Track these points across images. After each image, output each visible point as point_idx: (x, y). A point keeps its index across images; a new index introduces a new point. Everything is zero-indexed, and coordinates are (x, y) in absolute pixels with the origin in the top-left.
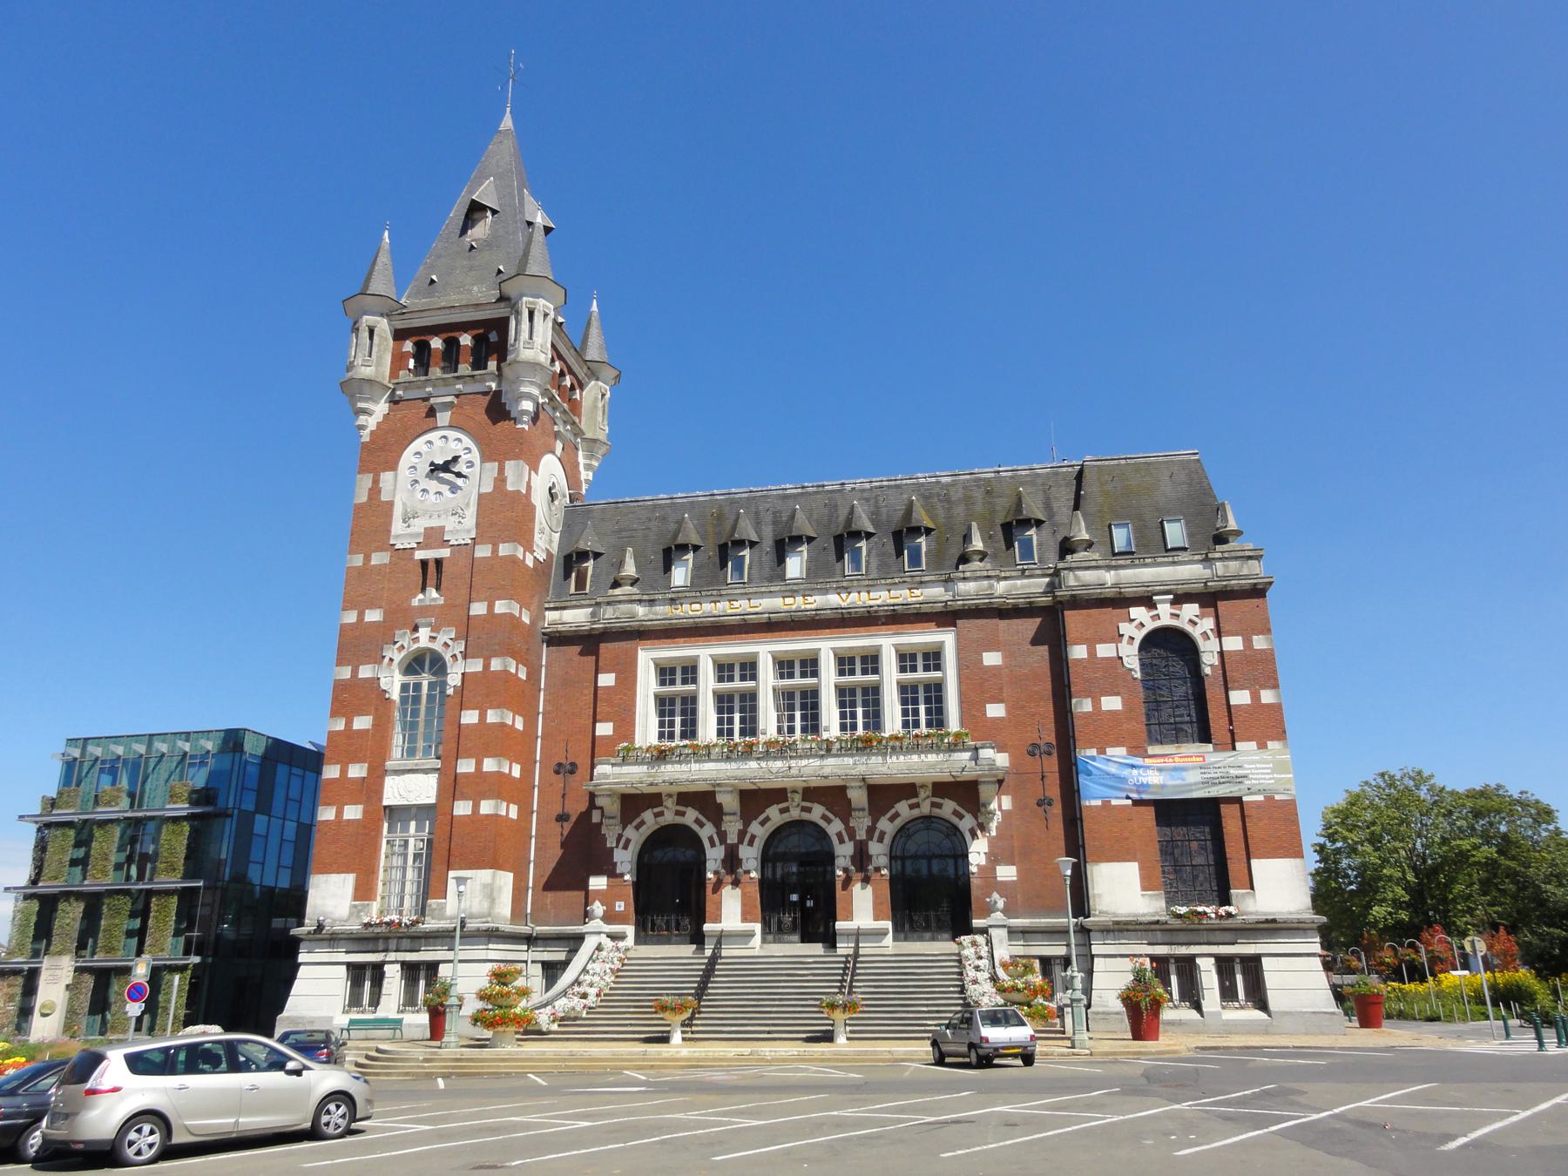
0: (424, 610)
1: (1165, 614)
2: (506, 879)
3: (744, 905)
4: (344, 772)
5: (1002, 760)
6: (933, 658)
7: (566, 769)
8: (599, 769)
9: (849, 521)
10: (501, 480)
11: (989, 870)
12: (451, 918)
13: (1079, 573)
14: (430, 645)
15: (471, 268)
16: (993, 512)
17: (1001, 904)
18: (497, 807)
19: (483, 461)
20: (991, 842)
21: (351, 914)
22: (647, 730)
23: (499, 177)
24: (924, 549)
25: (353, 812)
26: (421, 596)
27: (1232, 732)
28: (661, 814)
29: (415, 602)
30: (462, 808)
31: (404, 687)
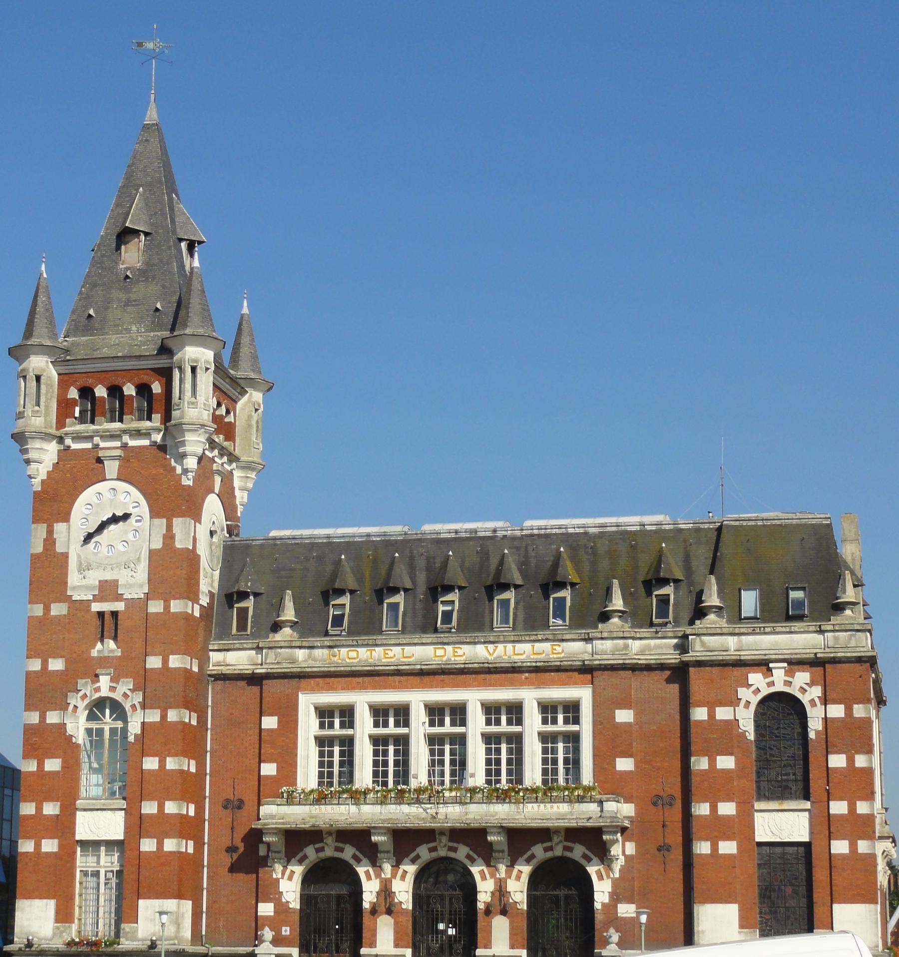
0: (104, 661)
1: (779, 681)
2: (187, 905)
3: (396, 932)
4: (39, 809)
5: (627, 810)
6: (572, 710)
7: (234, 805)
8: (265, 810)
9: (498, 572)
10: (169, 537)
11: (610, 908)
12: (142, 940)
13: (705, 639)
14: (111, 695)
15: (128, 303)
16: (636, 567)
17: (615, 937)
18: (179, 845)
19: (151, 518)
20: (615, 883)
21: (54, 935)
22: (308, 775)
23: (149, 186)
24: (568, 603)
25: (50, 846)
26: (99, 646)
27: (828, 791)
28: (322, 849)
29: (94, 653)
30: (148, 845)
31: (89, 731)
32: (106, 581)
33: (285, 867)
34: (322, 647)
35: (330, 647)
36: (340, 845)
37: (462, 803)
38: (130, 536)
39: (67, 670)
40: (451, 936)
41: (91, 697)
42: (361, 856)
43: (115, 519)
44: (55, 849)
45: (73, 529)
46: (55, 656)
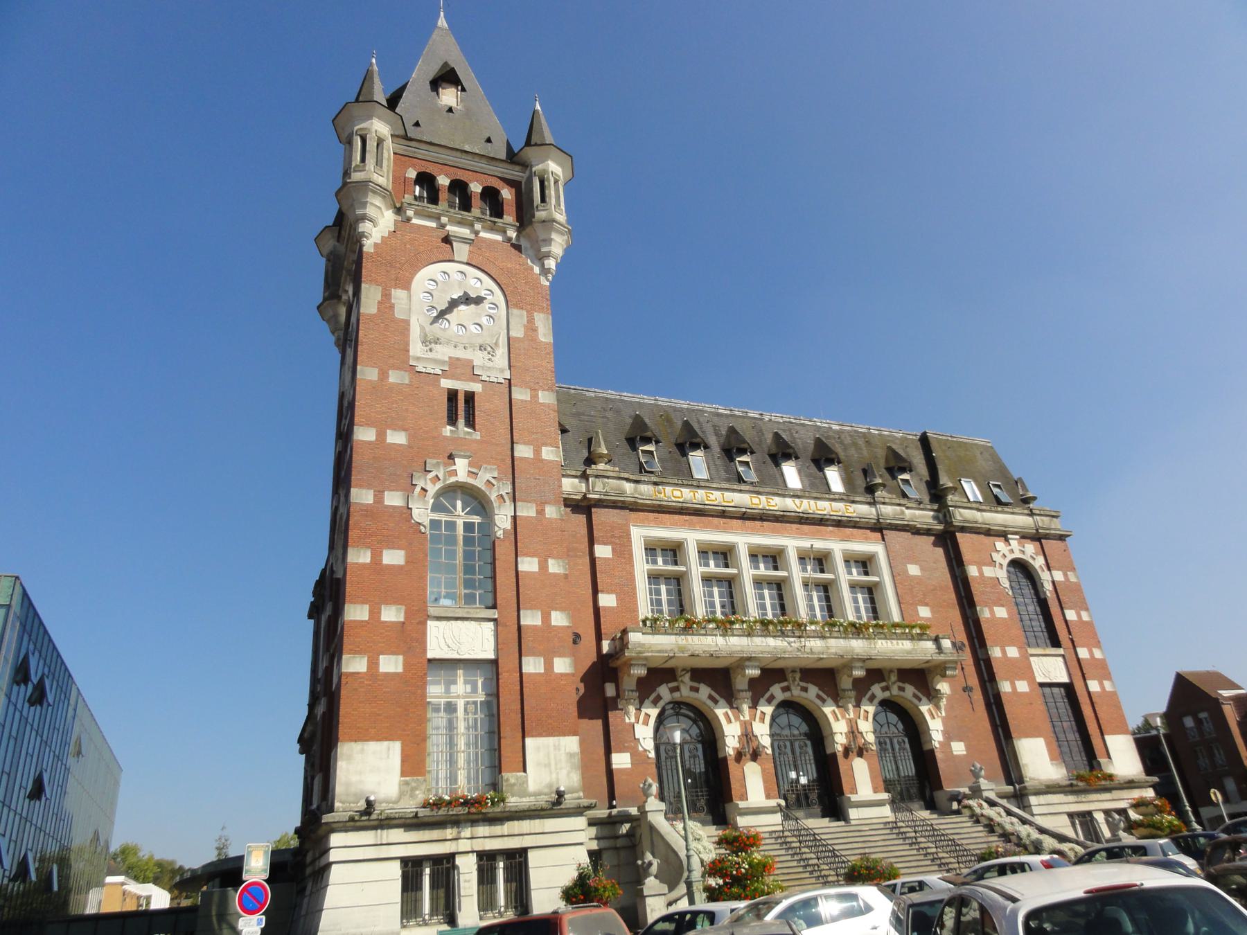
21: (401, 794)
25: (391, 664)
32: (458, 359)
33: (639, 709)
34: (648, 483)
35: (655, 484)
36: (695, 685)
37: (823, 637)
38: (484, 320)
39: (409, 446)
40: (804, 786)
41: (445, 480)
42: (717, 697)
43: (467, 300)
44: (400, 669)
45: (414, 298)
46: (396, 428)
